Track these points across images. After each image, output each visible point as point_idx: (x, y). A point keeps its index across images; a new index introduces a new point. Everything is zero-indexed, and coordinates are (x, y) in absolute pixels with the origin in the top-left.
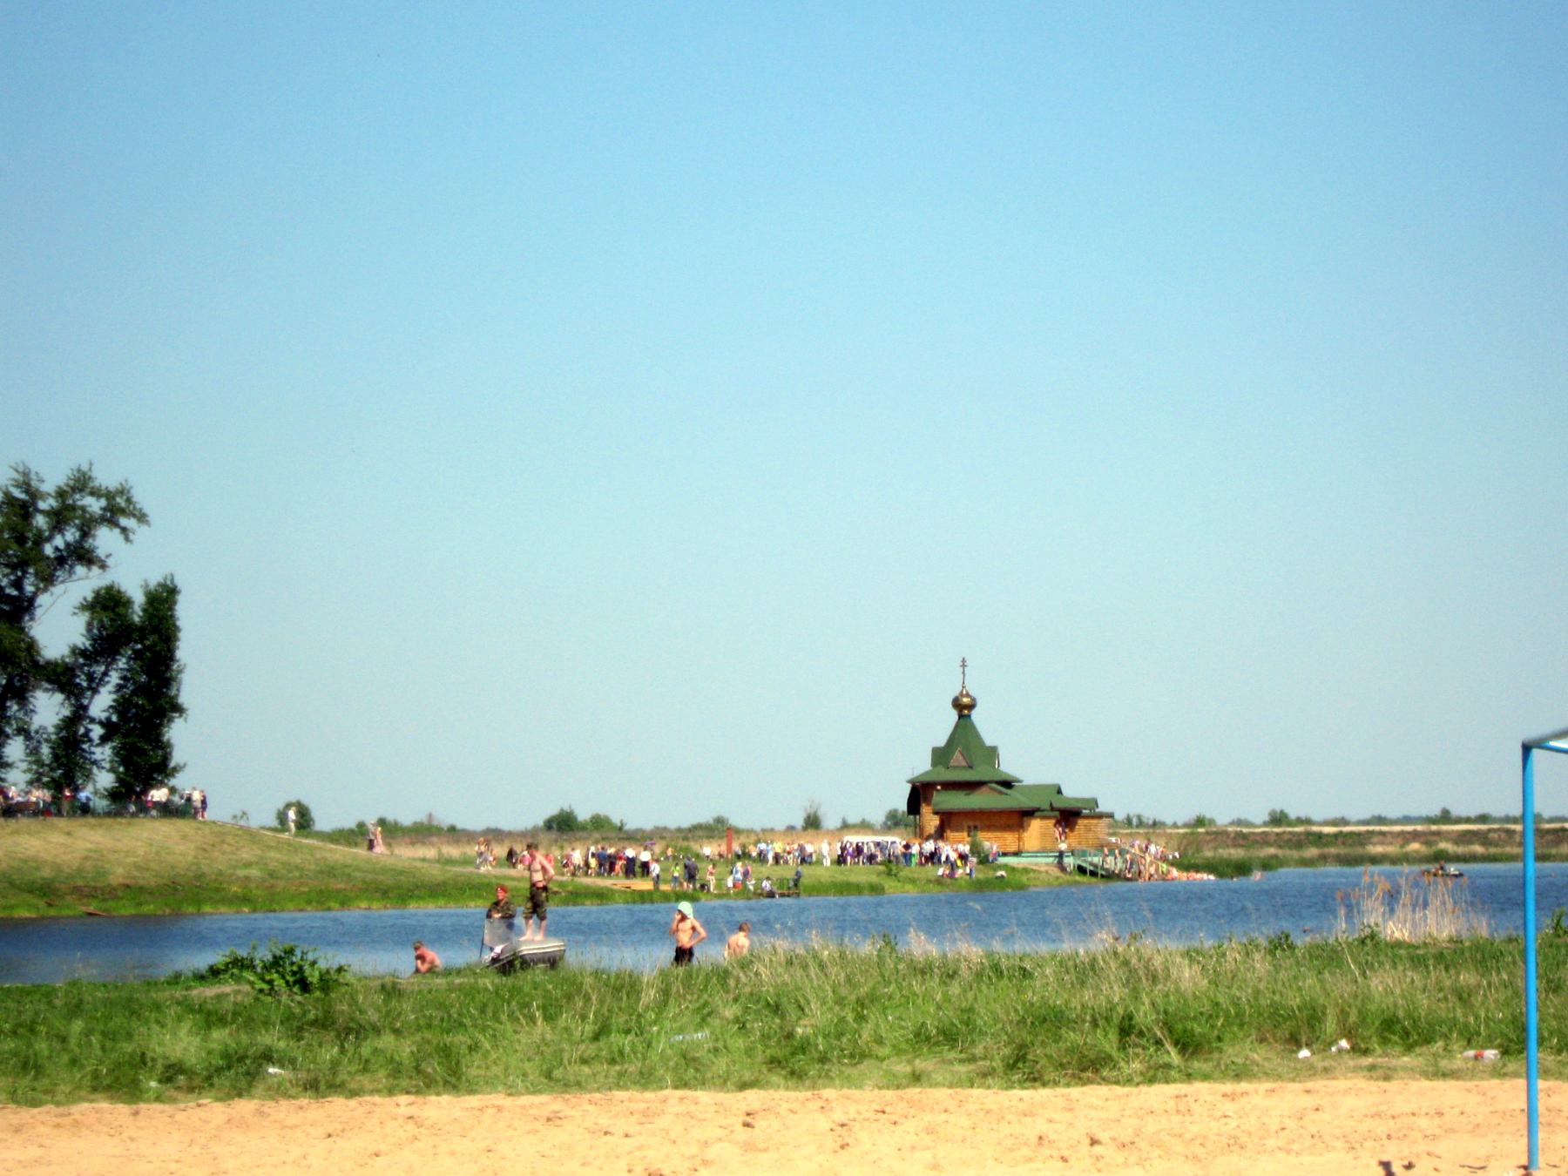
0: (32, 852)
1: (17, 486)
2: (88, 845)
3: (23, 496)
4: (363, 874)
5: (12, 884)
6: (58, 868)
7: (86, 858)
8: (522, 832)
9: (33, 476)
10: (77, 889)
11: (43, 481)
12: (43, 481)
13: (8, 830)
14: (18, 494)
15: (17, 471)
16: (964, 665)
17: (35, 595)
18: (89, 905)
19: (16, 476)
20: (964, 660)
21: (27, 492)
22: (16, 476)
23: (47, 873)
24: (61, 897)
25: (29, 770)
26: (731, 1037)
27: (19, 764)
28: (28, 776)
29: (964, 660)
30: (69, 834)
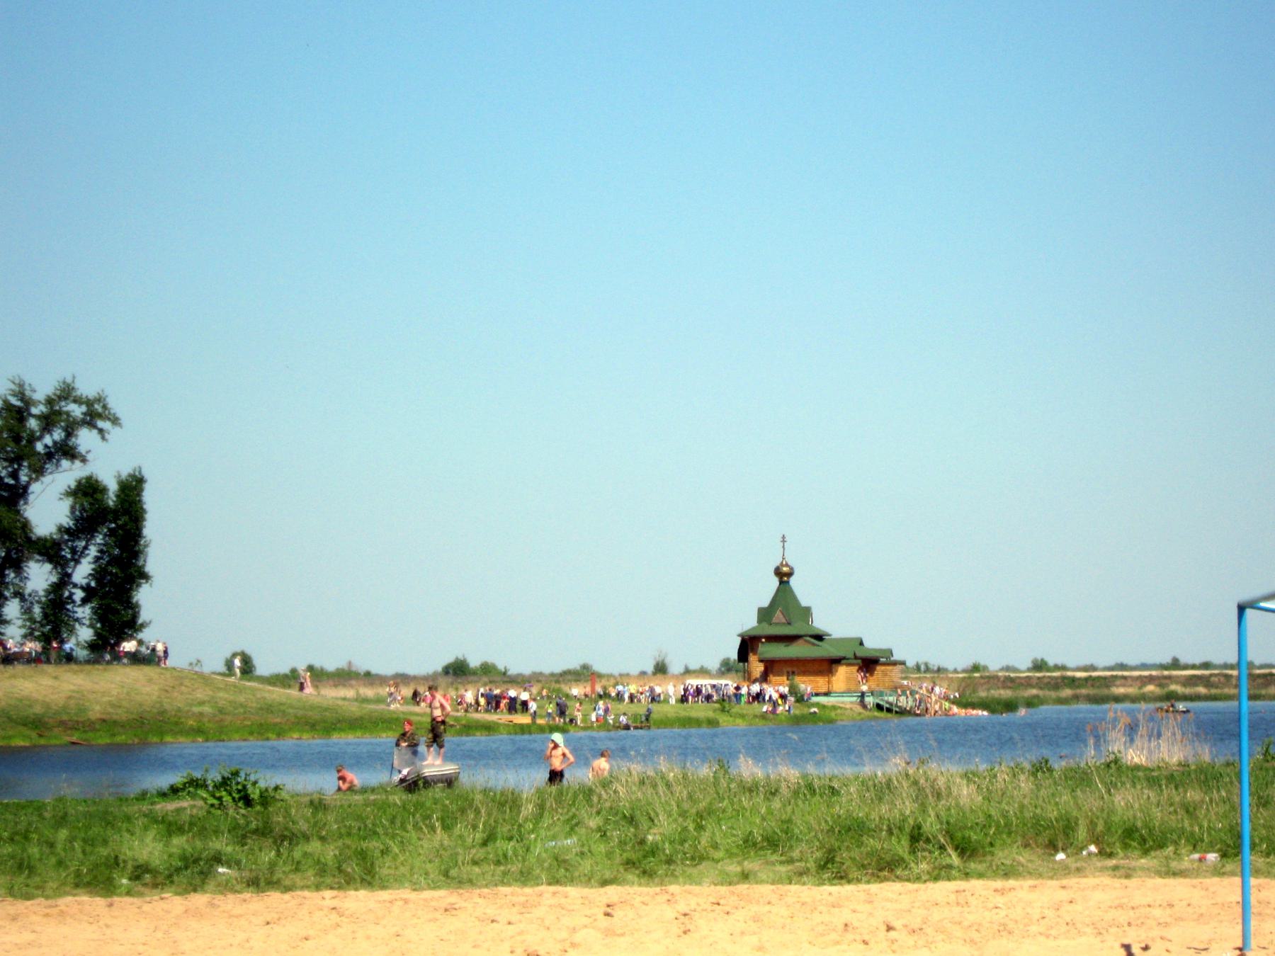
0: (26, 693)
1: (14, 395)
3: (18, 403)
5: (10, 719)
6: (47, 706)
9: (27, 387)
10: (62, 723)
11: (35, 391)
12: (35, 391)
13: (7, 675)
14: (15, 401)
15: (14, 383)
18: (73, 736)
19: (13, 387)
21: (22, 400)
22: (13, 387)
23: (38, 710)
24: (50, 729)
25: (23, 626)
27: (15, 621)
28: (23, 631)
30: (56, 678)
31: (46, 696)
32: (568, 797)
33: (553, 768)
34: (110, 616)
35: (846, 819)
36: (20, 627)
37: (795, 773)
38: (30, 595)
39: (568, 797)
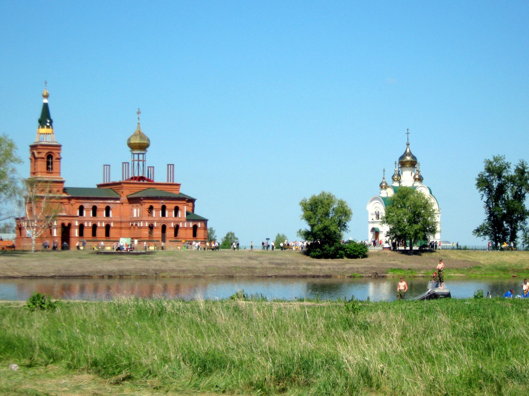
0: (505, 260)
1: (520, 165)
2: (522, 258)
3: (521, 168)
4: (328, 267)
5: (496, 268)
6: (510, 264)
7: (519, 262)
8: (427, 252)
9: (525, 163)
10: (513, 270)
11: (527, 164)
12: (527, 164)
13: (501, 254)
14: (520, 167)
15: (520, 161)
16: (384, 171)
17: (525, 193)
18: (515, 274)
19: (520, 162)
20: (384, 170)
21: (523, 167)
22: (520, 162)
23: (507, 265)
24: (508, 272)
25: (523, 239)
26: (38, 385)
27: (520, 237)
28: (523, 240)
29: (384, 170)
30: (517, 255)
31: (511, 261)
32: (255, 368)
33: (21, 179)
34: (504, 222)
35: (310, 240)
36: (522, 239)
37: (15, 367)
38: (526, 229)
39: (255, 368)
